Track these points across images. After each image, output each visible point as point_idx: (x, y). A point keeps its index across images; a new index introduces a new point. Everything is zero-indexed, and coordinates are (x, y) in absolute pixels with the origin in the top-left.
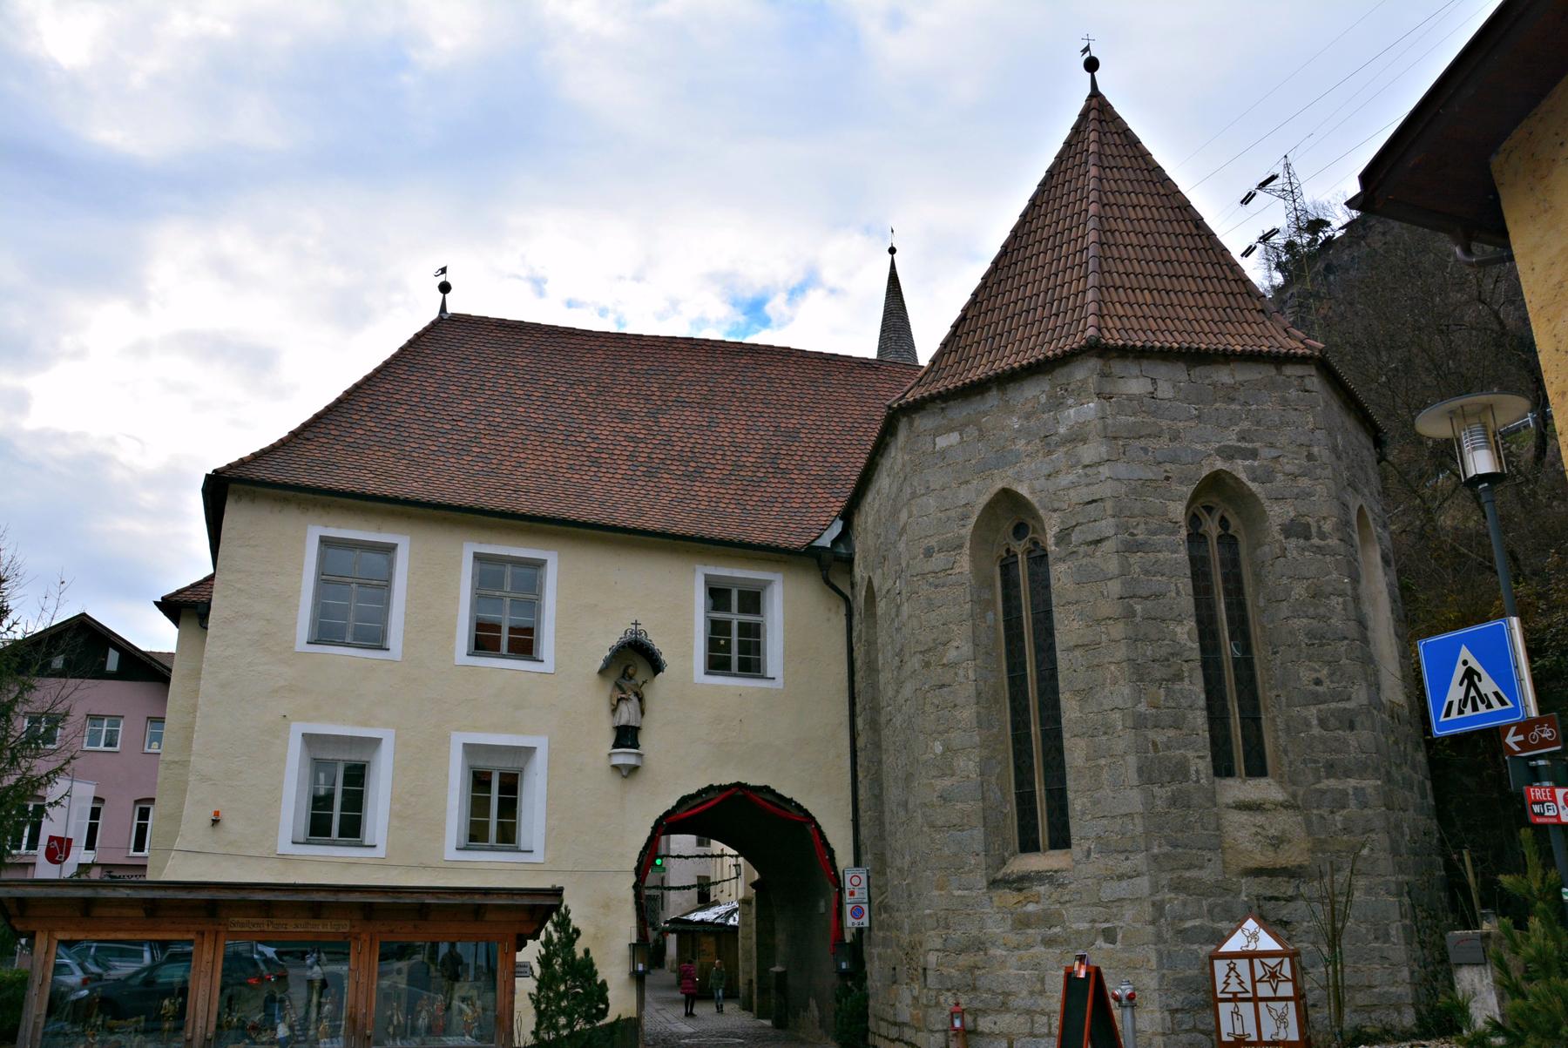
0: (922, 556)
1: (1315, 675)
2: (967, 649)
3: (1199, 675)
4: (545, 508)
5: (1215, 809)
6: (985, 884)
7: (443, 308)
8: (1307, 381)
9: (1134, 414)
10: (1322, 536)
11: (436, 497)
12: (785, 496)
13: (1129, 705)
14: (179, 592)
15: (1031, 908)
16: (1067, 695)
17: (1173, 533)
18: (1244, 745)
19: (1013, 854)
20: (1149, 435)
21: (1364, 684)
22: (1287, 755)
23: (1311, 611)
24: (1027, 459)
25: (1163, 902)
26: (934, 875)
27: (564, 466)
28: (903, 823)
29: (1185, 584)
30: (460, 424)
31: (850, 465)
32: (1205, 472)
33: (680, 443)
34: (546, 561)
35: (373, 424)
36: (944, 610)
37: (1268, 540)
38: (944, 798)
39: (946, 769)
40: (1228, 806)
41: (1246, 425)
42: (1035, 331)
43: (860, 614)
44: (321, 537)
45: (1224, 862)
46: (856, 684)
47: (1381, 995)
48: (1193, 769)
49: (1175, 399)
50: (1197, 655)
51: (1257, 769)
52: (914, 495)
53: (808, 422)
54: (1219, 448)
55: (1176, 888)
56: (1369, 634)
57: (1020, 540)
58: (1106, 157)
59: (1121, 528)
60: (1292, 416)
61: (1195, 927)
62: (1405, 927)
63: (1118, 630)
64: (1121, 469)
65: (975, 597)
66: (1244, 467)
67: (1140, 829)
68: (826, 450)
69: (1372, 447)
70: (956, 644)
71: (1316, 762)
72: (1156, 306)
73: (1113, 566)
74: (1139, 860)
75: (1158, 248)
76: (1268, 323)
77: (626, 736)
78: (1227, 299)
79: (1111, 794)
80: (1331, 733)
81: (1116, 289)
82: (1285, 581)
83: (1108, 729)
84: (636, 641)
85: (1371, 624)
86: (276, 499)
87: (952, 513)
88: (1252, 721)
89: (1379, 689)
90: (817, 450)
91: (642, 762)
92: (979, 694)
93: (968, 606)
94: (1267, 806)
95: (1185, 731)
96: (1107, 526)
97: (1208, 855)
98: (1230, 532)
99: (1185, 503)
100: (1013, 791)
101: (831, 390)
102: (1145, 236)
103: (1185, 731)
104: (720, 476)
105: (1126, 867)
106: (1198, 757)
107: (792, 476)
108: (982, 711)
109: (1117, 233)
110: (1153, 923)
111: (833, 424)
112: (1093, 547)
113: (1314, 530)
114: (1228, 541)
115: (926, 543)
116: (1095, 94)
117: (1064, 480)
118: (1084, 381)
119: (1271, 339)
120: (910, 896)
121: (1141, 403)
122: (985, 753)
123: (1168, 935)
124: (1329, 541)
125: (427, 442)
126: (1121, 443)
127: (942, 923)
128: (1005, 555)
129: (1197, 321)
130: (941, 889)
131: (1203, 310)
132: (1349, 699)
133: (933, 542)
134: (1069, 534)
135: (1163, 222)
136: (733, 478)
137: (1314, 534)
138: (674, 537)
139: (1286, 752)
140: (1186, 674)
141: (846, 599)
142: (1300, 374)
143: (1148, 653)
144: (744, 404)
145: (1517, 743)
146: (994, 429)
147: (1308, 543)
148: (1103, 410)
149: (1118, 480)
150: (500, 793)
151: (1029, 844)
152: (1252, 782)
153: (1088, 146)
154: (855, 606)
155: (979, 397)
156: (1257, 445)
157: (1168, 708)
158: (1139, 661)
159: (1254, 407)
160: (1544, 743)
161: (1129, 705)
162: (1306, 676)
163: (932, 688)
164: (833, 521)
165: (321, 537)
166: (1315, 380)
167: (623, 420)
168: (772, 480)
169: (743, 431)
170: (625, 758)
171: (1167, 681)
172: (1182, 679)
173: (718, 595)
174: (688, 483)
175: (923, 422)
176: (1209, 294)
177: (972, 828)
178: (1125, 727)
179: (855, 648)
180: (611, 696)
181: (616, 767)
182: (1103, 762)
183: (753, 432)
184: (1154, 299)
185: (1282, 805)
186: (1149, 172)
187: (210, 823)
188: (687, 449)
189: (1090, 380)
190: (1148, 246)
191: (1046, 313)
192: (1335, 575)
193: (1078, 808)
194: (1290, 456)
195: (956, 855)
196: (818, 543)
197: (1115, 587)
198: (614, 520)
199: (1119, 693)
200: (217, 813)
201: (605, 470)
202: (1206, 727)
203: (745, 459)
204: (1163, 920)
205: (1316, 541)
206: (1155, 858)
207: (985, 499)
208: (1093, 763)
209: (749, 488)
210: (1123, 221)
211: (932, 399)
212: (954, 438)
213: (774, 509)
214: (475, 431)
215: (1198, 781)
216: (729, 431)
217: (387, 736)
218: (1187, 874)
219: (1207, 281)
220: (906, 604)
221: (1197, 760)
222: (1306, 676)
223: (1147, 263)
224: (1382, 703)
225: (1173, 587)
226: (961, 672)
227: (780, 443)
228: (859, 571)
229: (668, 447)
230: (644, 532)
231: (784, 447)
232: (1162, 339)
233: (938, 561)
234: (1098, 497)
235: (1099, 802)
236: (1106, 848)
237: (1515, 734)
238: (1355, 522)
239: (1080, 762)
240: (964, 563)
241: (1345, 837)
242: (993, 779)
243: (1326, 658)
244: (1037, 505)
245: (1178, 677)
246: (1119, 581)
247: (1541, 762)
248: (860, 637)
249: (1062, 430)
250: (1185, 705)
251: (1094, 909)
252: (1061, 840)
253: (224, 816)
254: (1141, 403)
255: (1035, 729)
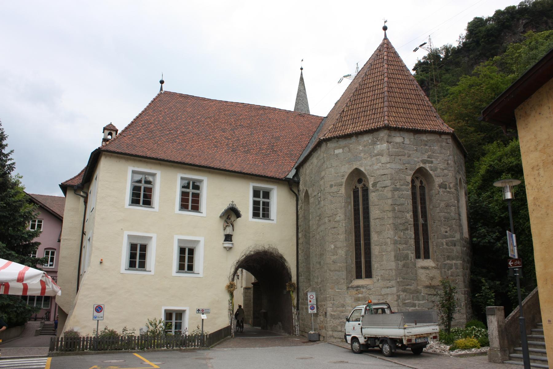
0: (329, 187)
1: (446, 230)
2: (343, 217)
3: (413, 229)
4: (203, 163)
5: (415, 268)
6: (346, 288)
7: (161, 89)
8: (448, 140)
9: (398, 148)
10: (450, 188)
11: (169, 158)
12: (277, 160)
13: (393, 237)
14: (67, 181)
15: (360, 295)
16: (374, 233)
17: (407, 185)
18: (424, 249)
19: (354, 279)
20: (402, 155)
21: (459, 233)
22: (436, 253)
23: (446, 211)
24: (364, 160)
25: (400, 295)
26: (330, 285)
27: (206, 147)
28: (318, 269)
29: (410, 201)
30: (172, 131)
31: (296, 150)
32: (417, 168)
33: (242, 141)
34: (203, 180)
35: (144, 131)
36: (335, 204)
37: (435, 188)
38: (334, 262)
39: (335, 253)
40: (419, 268)
41: (430, 153)
42: (367, 119)
43: (302, 201)
44: (132, 170)
45: (417, 284)
46: (299, 223)
47: (458, 322)
48: (410, 257)
49: (410, 144)
50: (412, 223)
51: (427, 256)
52: (327, 168)
53: (283, 134)
54: (422, 160)
55: (403, 291)
56: (461, 217)
57: (359, 184)
58: (389, 61)
59: (393, 183)
60: (443, 151)
61: (408, 302)
62: (465, 303)
63: (390, 214)
64: (393, 166)
65: (346, 201)
66: (429, 166)
67: (394, 274)
68: (288, 144)
69: (463, 158)
70: (339, 215)
71: (444, 255)
72: (405, 114)
73: (390, 195)
74: (393, 283)
75: (405, 94)
76: (437, 121)
77: (228, 238)
78: (425, 112)
79: (386, 263)
80: (449, 247)
81: (393, 107)
82: (439, 201)
83: (386, 244)
84: (233, 208)
85: (461, 215)
86: (117, 157)
87: (339, 174)
88: (426, 243)
89: (462, 234)
90: (286, 144)
91: (233, 246)
92: (346, 231)
93: (344, 204)
94: (430, 268)
95: (408, 245)
96: (388, 183)
97: (413, 282)
98: (423, 185)
99: (411, 176)
100: (355, 260)
101: (289, 123)
102: (401, 89)
103: (408, 245)
104: (256, 152)
105: (390, 284)
106: (412, 253)
107: (278, 153)
108: (347, 236)
109: (393, 88)
110: (397, 301)
111: (290, 135)
112: (384, 188)
113: (448, 186)
114: (422, 188)
115: (330, 183)
116: (386, 38)
117: (375, 167)
118: (383, 137)
119: (438, 126)
120: (321, 290)
121: (400, 145)
122: (347, 249)
123: (401, 305)
124: (452, 190)
125: (162, 138)
126: (393, 157)
127: (332, 299)
128: (355, 188)
129: (417, 119)
130: (332, 289)
131: (419, 115)
132: (455, 237)
133: (333, 183)
134: (376, 184)
135: (407, 85)
136: (260, 153)
137: (448, 188)
138: (244, 173)
139: (436, 252)
140: (409, 228)
141: (296, 195)
142: (446, 138)
143: (399, 222)
144: (262, 127)
145: (511, 264)
146: (354, 149)
147: (446, 190)
148: (389, 147)
149: (392, 168)
150: (188, 255)
151: (359, 276)
152: (426, 260)
153: (384, 57)
154: (299, 198)
155: (349, 138)
156: (433, 159)
157: (404, 238)
158: (396, 224)
159: (432, 148)
160: (518, 265)
161: (393, 237)
162: (443, 230)
163: (331, 228)
164: (292, 169)
165: (132, 170)
166: (451, 140)
167: (224, 132)
168: (272, 154)
169: (262, 137)
170: (228, 244)
171: (404, 230)
172: (408, 230)
173: (256, 193)
174: (246, 154)
175: (330, 145)
176: (420, 110)
177: (342, 271)
178: (391, 243)
179: (299, 211)
180: (224, 226)
181: (225, 247)
182: (384, 253)
183: (265, 137)
184: (404, 111)
185: (434, 268)
186: (402, 67)
187: (100, 263)
188: (245, 143)
189: (385, 137)
190: (402, 93)
191: (371, 113)
192: (453, 200)
193: (376, 267)
194: (442, 163)
195: (337, 279)
196: (288, 177)
197: (390, 202)
198: (225, 167)
199: (390, 233)
200: (102, 260)
201: (219, 149)
202: (414, 244)
203: (263, 147)
204: (399, 300)
205: (448, 190)
206: (398, 282)
207: (350, 171)
208: (380, 254)
209: (265, 157)
210: (395, 84)
211: (334, 138)
212: (340, 151)
213: (273, 164)
214: (197, 146)
215: (411, 260)
216: (257, 137)
217: (154, 236)
218: (407, 287)
219: (420, 106)
220: (323, 201)
221: (411, 254)
222: (443, 230)
223: (402, 99)
224: (463, 238)
225: (407, 202)
226: (341, 224)
227: (274, 141)
228: (301, 187)
229: (238, 142)
230: (235, 172)
231: (275, 143)
232: (407, 125)
233: (334, 189)
234: (386, 173)
235: (382, 265)
236: (384, 279)
237: (511, 262)
238: (458, 183)
239: (377, 253)
240: (343, 190)
241: (451, 278)
242: (349, 257)
243: (449, 225)
244: (367, 174)
245: (407, 229)
246: (391, 199)
247: (517, 269)
248: (301, 208)
249: (375, 152)
250: (408, 237)
251: (379, 296)
252: (369, 275)
253: (103, 261)
254: (400, 145)
255: (362, 242)
